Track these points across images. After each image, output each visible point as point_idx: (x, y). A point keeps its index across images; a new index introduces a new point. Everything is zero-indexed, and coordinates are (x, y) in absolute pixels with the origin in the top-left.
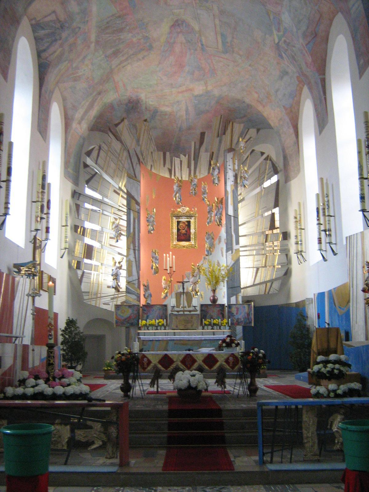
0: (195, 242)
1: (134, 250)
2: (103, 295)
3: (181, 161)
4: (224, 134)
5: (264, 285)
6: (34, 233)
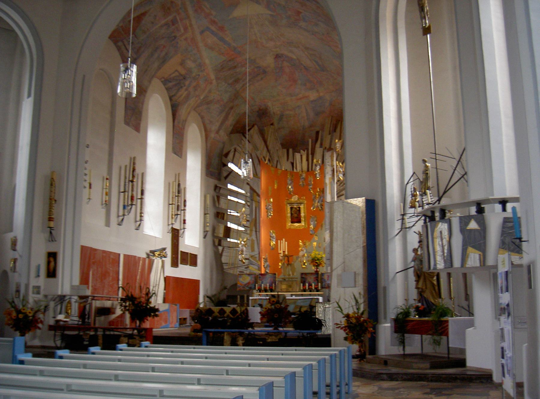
0: (305, 224)
1: (256, 231)
3: (301, 156)
4: (335, 131)
6: (171, 226)
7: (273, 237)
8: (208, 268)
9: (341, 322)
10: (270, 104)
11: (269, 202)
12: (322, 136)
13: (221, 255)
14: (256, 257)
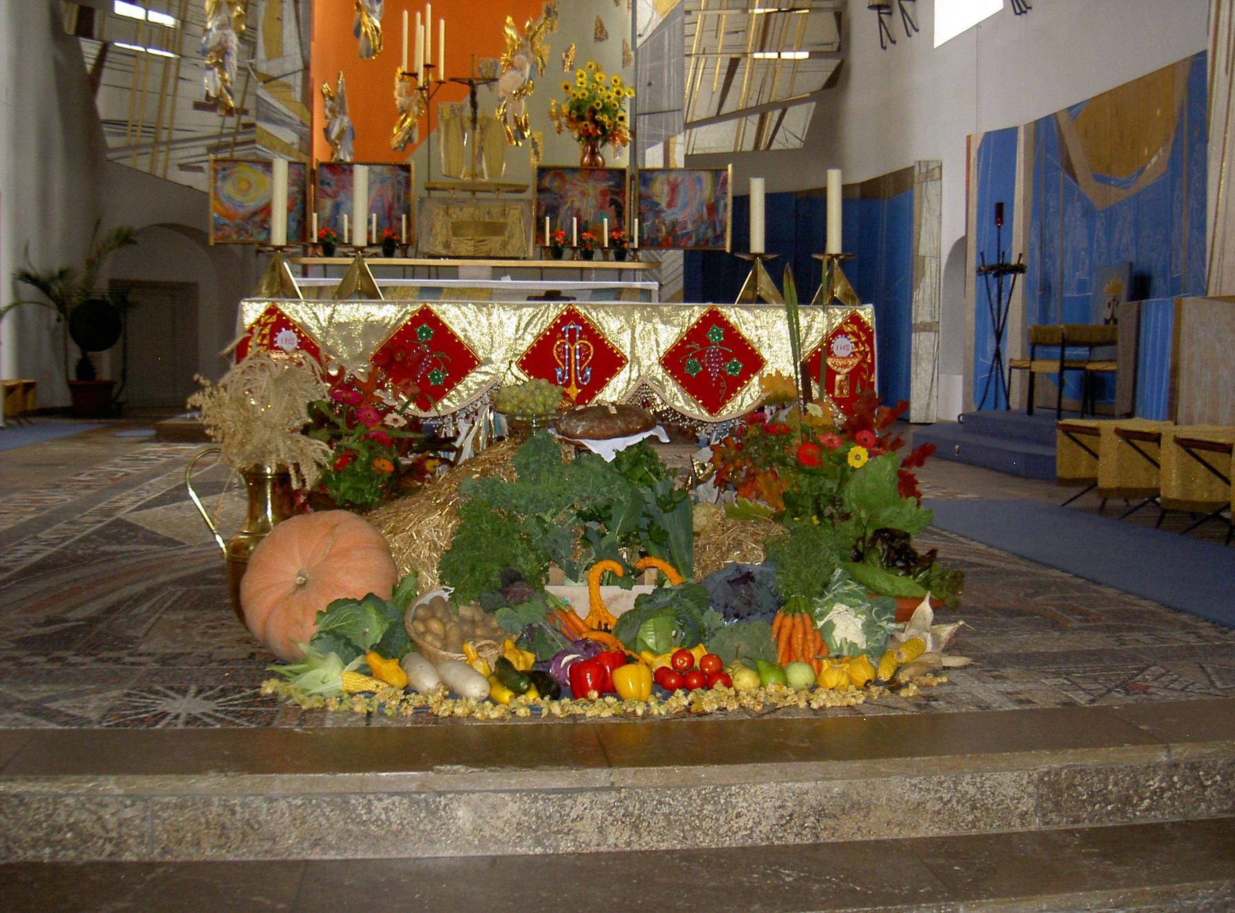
2: (178, 135)
5: (755, 118)
8: (31, 143)
13: (93, 82)
14: (289, 87)
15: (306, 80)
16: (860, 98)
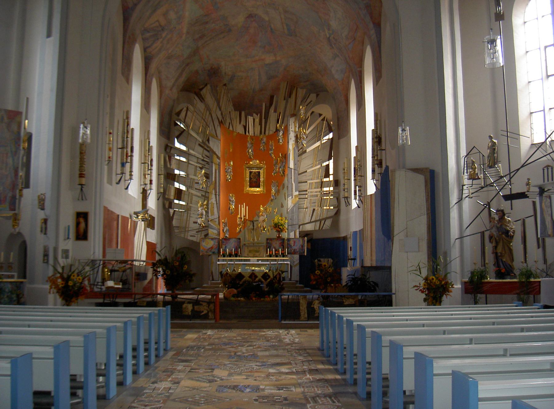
0: (263, 188)
1: (216, 195)
2: (190, 229)
3: (254, 120)
4: (290, 97)
6: (143, 187)
7: (232, 201)
9: (420, 284)
10: (223, 63)
11: (229, 165)
12: (277, 102)
13: (172, 218)
14: (215, 221)
15: (219, 220)
16: (342, 217)
